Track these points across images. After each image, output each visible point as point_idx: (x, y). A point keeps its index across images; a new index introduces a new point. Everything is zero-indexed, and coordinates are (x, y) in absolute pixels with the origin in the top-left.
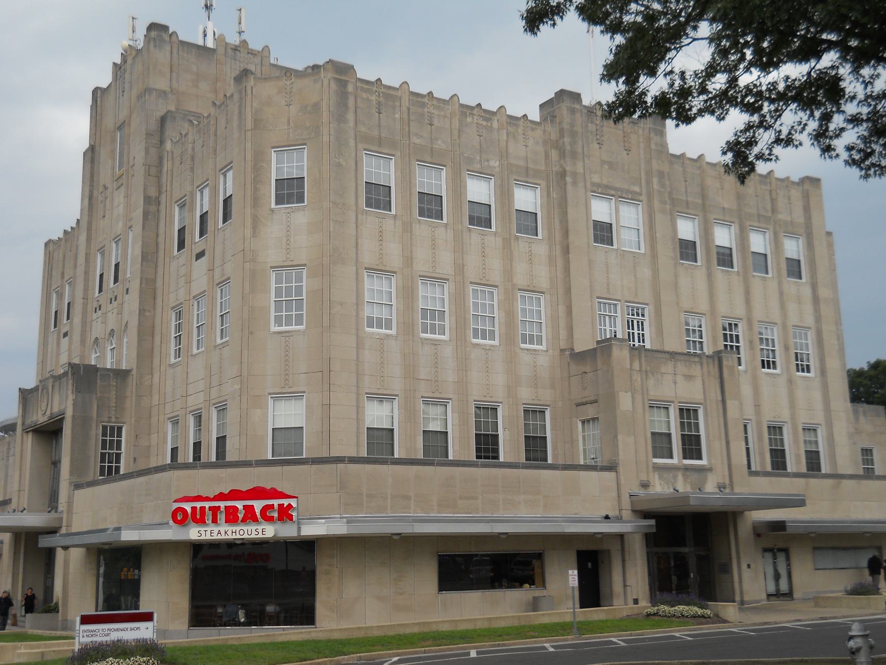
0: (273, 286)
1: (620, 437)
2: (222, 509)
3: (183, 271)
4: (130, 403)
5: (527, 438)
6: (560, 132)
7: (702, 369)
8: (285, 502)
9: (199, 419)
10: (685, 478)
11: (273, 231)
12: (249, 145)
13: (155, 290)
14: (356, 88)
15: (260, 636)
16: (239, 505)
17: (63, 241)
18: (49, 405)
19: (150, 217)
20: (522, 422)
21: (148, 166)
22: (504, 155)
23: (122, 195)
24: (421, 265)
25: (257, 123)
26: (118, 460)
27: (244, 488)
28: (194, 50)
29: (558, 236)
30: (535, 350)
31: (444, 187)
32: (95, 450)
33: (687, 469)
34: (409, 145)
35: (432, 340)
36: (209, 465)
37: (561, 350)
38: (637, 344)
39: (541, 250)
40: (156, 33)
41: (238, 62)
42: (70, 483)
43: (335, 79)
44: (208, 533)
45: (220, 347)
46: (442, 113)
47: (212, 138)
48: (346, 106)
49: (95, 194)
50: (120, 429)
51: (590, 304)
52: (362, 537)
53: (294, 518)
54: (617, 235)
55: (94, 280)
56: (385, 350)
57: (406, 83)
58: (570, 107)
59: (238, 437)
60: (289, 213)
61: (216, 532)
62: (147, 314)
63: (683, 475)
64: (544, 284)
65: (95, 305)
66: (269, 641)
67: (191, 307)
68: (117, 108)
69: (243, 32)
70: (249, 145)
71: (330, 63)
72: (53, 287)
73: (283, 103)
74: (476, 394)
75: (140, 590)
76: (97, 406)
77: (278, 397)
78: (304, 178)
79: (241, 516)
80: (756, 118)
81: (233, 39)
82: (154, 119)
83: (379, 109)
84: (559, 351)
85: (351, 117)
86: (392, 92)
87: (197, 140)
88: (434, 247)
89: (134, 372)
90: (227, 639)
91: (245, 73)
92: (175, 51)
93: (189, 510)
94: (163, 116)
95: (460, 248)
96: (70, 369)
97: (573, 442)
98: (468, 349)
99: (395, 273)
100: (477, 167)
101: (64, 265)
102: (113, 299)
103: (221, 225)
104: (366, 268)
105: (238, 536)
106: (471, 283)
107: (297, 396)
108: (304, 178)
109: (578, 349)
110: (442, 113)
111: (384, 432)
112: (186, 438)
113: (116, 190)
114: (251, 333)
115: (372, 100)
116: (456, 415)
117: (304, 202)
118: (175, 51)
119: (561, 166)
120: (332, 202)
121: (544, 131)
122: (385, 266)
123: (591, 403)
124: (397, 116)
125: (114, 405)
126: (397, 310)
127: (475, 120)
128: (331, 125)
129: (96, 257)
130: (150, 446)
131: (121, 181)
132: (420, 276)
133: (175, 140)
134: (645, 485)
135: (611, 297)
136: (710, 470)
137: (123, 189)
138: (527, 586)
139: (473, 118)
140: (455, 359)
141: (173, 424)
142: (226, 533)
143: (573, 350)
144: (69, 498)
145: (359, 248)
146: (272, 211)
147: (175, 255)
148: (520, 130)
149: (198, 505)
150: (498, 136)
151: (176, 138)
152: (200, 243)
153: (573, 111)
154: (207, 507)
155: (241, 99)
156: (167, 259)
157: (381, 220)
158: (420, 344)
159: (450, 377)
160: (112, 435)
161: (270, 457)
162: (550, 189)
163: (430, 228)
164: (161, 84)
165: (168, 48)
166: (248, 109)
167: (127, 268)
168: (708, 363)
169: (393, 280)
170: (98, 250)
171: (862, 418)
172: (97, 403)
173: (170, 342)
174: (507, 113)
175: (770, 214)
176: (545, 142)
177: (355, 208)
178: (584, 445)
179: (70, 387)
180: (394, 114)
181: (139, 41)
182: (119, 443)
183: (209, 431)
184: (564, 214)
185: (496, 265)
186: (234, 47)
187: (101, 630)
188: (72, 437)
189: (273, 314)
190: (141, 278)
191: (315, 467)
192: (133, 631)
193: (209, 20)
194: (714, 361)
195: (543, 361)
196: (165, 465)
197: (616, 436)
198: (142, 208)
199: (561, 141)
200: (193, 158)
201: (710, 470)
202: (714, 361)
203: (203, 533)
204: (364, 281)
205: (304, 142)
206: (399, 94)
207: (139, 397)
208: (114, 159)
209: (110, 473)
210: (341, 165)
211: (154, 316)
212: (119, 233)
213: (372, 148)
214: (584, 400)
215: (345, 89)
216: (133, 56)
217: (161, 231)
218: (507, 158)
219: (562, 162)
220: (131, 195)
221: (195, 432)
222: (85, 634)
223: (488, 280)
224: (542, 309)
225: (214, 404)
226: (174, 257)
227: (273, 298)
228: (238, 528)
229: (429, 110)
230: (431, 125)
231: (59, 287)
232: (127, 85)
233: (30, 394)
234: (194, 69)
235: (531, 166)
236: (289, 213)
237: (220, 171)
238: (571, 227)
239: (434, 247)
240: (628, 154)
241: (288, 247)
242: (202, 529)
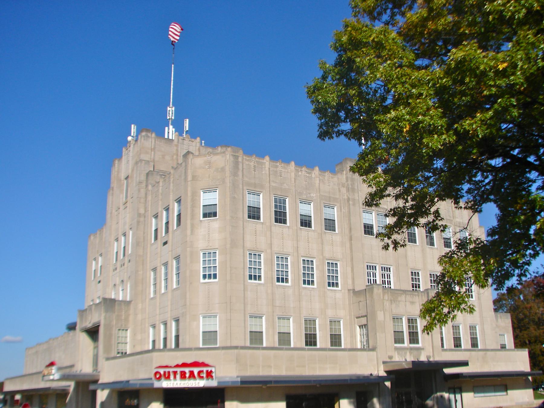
1: (378, 334)
4: (131, 318)
7: (419, 298)
8: (209, 369)
10: (411, 353)
11: (201, 231)
25: (194, 178)
29: (347, 231)
33: (411, 349)
34: (270, 187)
36: (171, 350)
38: (387, 286)
43: (232, 155)
46: (286, 171)
51: (362, 266)
53: (214, 377)
63: (410, 352)
74: (305, 314)
78: (216, 204)
79: (187, 375)
80: (532, 255)
85: (240, 173)
91: (188, 153)
93: (162, 373)
106: (302, 256)
109: (357, 289)
110: (286, 171)
114: (191, 283)
121: (338, 178)
127: (303, 174)
132: (276, 253)
134: (390, 357)
135: (373, 262)
136: (423, 349)
139: (302, 172)
143: (354, 290)
145: (245, 239)
146: (201, 221)
149: (167, 370)
152: (165, 237)
161: (201, 346)
166: (189, 171)
168: (421, 295)
171: (499, 320)
175: (452, 219)
177: (242, 219)
180: (262, 171)
191: (223, 351)
194: (425, 294)
197: (376, 334)
201: (423, 349)
202: (425, 294)
205: (217, 186)
218: (319, 192)
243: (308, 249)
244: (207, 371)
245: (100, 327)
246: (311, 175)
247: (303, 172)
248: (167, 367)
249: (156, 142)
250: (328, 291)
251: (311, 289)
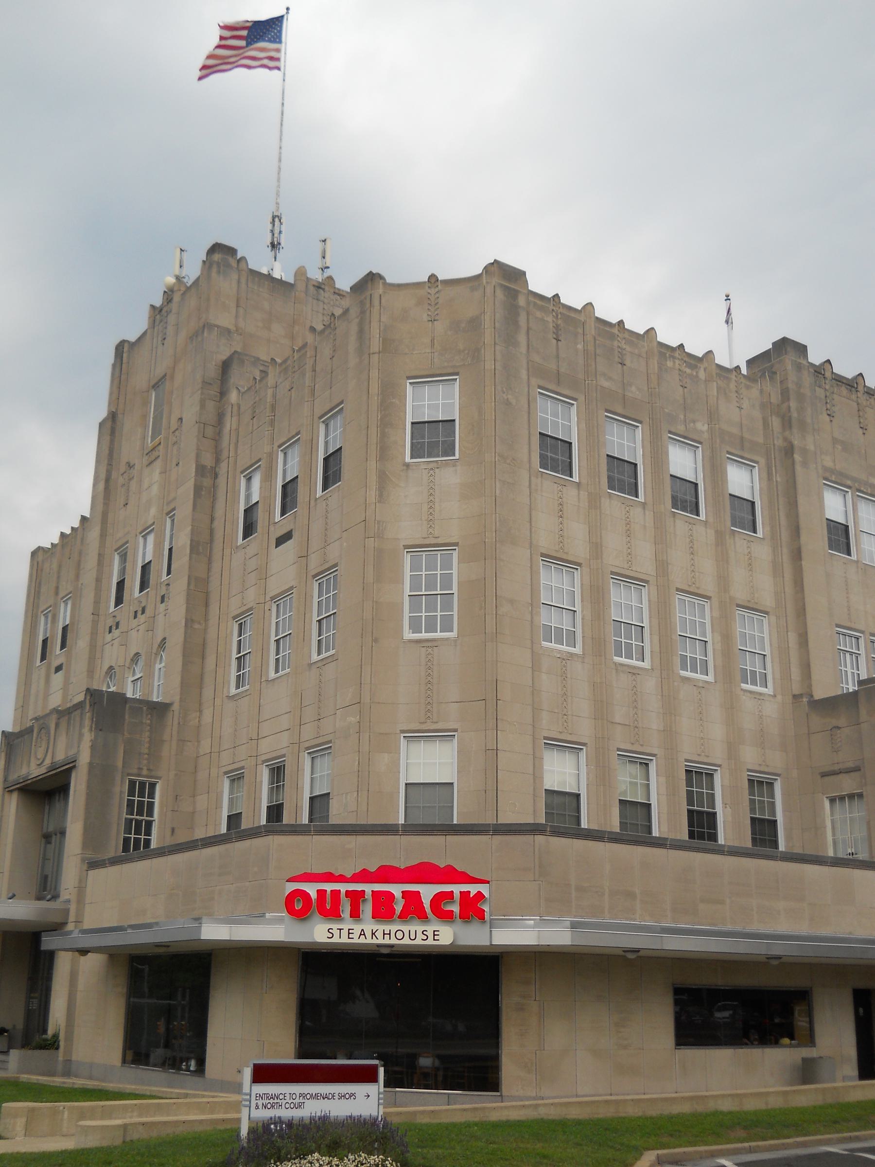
0: (408, 573)
2: (368, 895)
3: (252, 564)
4: (168, 751)
5: (753, 820)
6: (782, 394)
8: (473, 889)
9: (277, 772)
12: (374, 374)
13: (207, 594)
14: (528, 303)
15: (465, 1110)
16: (396, 890)
17: (59, 547)
18: (50, 751)
19: (203, 493)
20: (746, 796)
21: (202, 424)
22: (712, 416)
23: (158, 471)
24: (613, 559)
26: (148, 833)
27: (402, 864)
28: (266, 283)
29: (785, 535)
30: (761, 694)
31: (640, 452)
32: (118, 814)
35: (628, 666)
37: (795, 697)
39: (763, 553)
40: (220, 255)
41: (321, 303)
42: (83, 860)
43: (502, 286)
44: (345, 933)
45: (319, 664)
46: (636, 351)
47: (308, 375)
48: (516, 323)
49: (114, 475)
50: (153, 786)
52: (569, 953)
54: (856, 542)
55: (109, 590)
56: (569, 676)
57: (591, 304)
58: (796, 361)
59: (356, 794)
60: (432, 469)
61: (357, 932)
62: (196, 626)
64: (767, 600)
65: (110, 622)
66: (477, 1119)
67: (267, 613)
68: (153, 362)
69: (328, 268)
70: (374, 374)
71: (495, 265)
72: (41, 609)
73: (425, 317)
75: (207, 1023)
76: (124, 752)
77: (415, 735)
78: (454, 420)
79: (399, 908)
81: (315, 275)
82: (214, 363)
83: (557, 334)
84: (791, 697)
85: (522, 338)
86: (573, 315)
87: (281, 383)
88: (628, 533)
89: (176, 707)
90: (415, 1113)
92: (243, 280)
93: (314, 895)
94: (226, 360)
95: (661, 539)
96: (88, 698)
97: (817, 829)
98: (676, 684)
99: (580, 565)
100: (681, 428)
101: (59, 577)
102: (140, 612)
103: (319, 493)
104: (542, 555)
105: (394, 941)
107: (444, 735)
108: (454, 420)
109: (819, 694)
111: (567, 799)
112: (256, 799)
113: (147, 466)
114: (376, 640)
115: (547, 321)
116: (663, 780)
117: (454, 455)
118: (243, 280)
119: (785, 439)
120: (499, 455)
121: (761, 391)
122: (567, 553)
123: (848, 771)
124: (580, 346)
125: (146, 751)
126: (583, 619)
127: (677, 366)
128: (498, 347)
129: (112, 560)
130: (194, 813)
131: (155, 454)
133: (242, 390)
137: (158, 464)
138: (786, 1041)
139: (674, 362)
140: (660, 697)
141: (233, 781)
142: (373, 934)
143: (812, 696)
144: (80, 881)
146: (407, 465)
147: (239, 544)
148: (732, 385)
149: (329, 887)
150: (706, 391)
151: (244, 388)
153: (799, 367)
154: (343, 891)
155: (363, 312)
156: (227, 552)
157: (560, 487)
158: (614, 671)
159: (654, 723)
160: (142, 795)
162: (772, 470)
163: (623, 506)
164: (225, 320)
165: (235, 276)
166: (375, 325)
167: (162, 569)
169: (577, 575)
170: (116, 550)
172: (125, 747)
173: (230, 665)
174: (716, 362)
176: (763, 406)
178: (834, 834)
179: (87, 722)
181: (187, 278)
182: (151, 805)
183: (298, 788)
184: (793, 504)
185: (707, 566)
186: (316, 284)
187: (288, 1096)
188: (87, 794)
189: (407, 614)
190: (189, 577)
191: (498, 839)
192: (343, 1101)
193: (275, 260)
195: (771, 710)
196: (260, 827)
198: (193, 480)
199: (785, 405)
200: (273, 408)
204: (540, 573)
205: (456, 371)
206: (582, 318)
207: (182, 741)
208: (145, 427)
209: (137, 847)
210: (510, 403)
211: (205, 630)
212: (150, 522)
213: (550, 387)
214: (836, 768)
215: (515, 301)
216: (182, 292)
217: (219, 512)
219: (787, 433)
220: (170, 470)
221: (271, 790)
222: (260, 1103)
223: (698, 588)
224: (766, 636)
225: (308, 748)
226: (237, 547)
227: (407, 592)
228: (394, 928)
229: (620, 345)
230: (623, 364)
231: (50, 606)
232: (170, 330)
233: (18, 738)
234: (266, 305)
235: (746, 435)
236: (432, 469)
237: (320, 418)
238: (802, 524)
239: (628, 533)
240: (864, 434)
241: (431, 517)
242: (335, 926)
243: (693, 571)
244: (464, 895)
245: (73, 775)
246: (697, 373)
247: (677, 362)
248: (329, 877)
249: (250, 285)
250: (742, 693)
251: (701, 685)
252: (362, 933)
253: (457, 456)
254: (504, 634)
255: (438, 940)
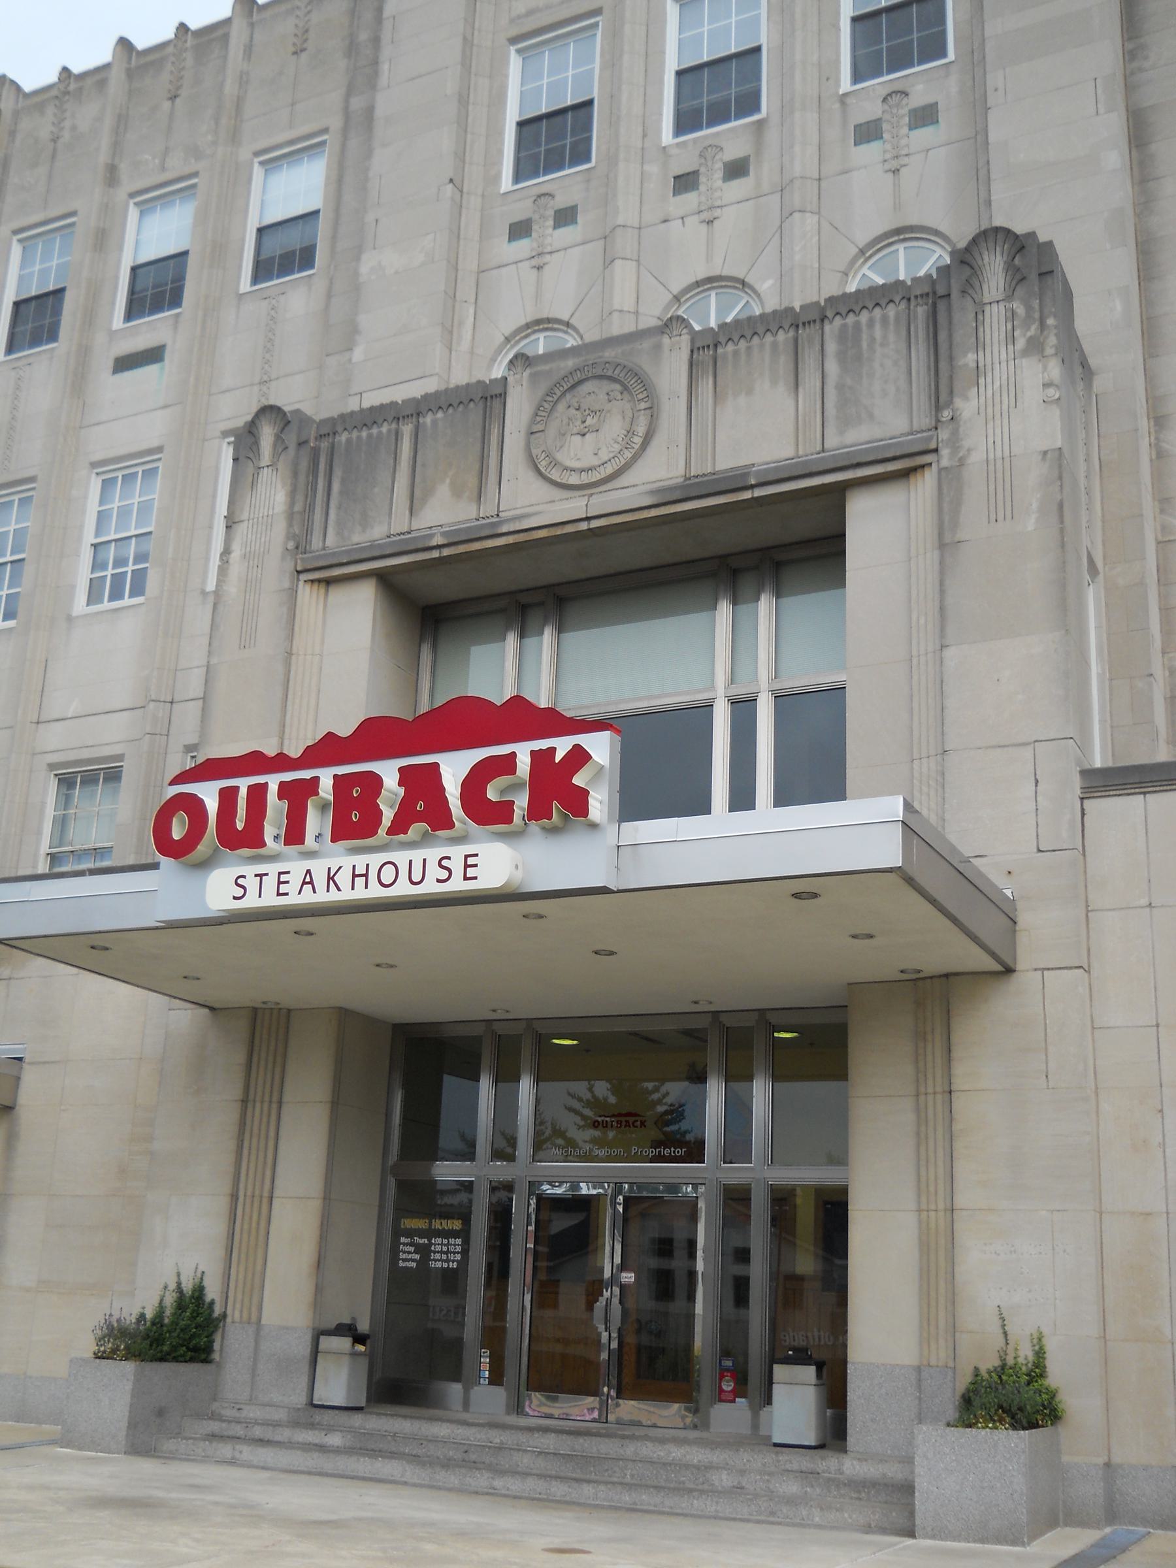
44: (270, 883)
61: (296, 878)
93: (212, 805)
142: (330, 878)
203: (251, 883)
252: (308, 879)
253: (951, 55)
254: (1157, 178)
255: (475, 878)
